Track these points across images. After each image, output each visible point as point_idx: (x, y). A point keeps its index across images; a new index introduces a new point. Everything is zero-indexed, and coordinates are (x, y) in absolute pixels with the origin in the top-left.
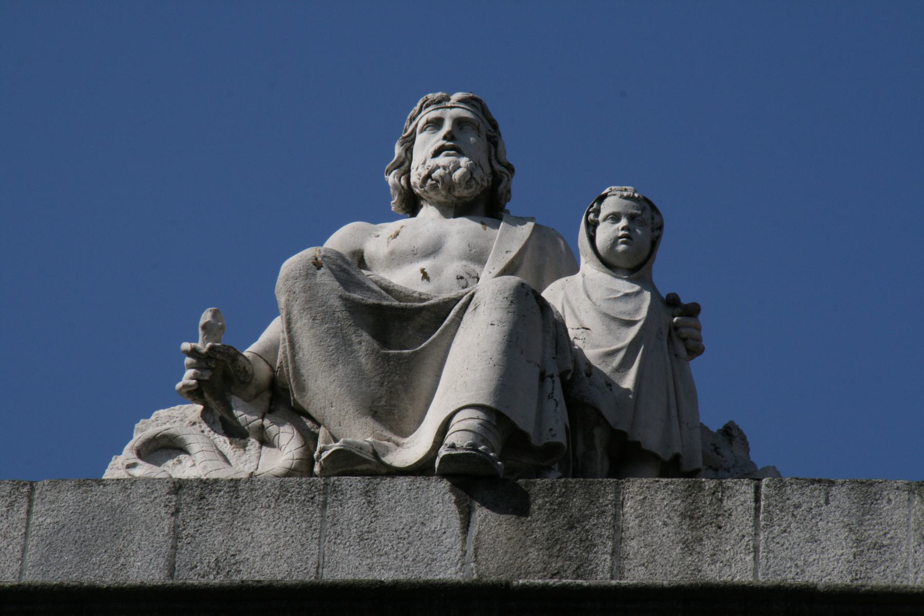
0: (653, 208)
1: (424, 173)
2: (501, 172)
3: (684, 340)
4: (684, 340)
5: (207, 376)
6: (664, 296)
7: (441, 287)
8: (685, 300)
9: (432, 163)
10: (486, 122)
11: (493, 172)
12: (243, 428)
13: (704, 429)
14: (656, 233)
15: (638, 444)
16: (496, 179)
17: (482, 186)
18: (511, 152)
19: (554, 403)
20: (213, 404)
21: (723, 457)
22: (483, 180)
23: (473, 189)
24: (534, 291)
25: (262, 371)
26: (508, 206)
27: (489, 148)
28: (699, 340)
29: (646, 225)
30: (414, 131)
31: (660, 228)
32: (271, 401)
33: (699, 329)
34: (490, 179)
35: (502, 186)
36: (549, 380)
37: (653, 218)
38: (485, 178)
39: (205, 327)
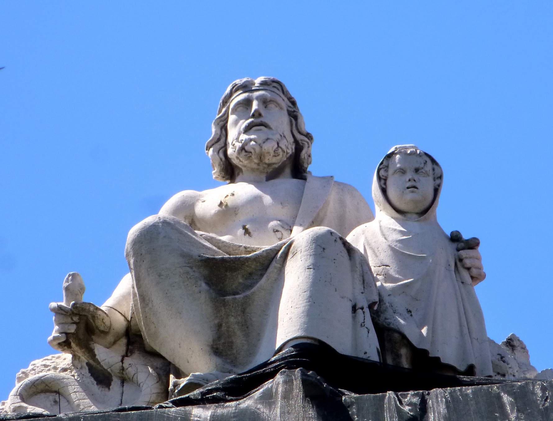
0: (433, 161)
1: (238, 145)
2: (301, 140)
3: (469, 269)
4: (469, 269)
5: (72, 329)
6: (449, 234)
7: (262, 244)
8: (466, 236)
9: (244, 137)
10: (286, 99)
11: (296, 141)
12: (106, 370)
13: (492, 342)
14: (438, 182)
15: (438, 359)
16: (299, 148)
17: (287, 153)
18: (308, 123)
19: (366, 330)
20: (80, 353)
21: (508, 364)
22: (288, 148)
23: (281, 156)
24: (341, 239)
25: (119, 322)
26: (310, 168)
27: (291, 122)
28: (480, 268)
29: (429, 176)
30: (227, 112)
31: (441, 177)
32: (129, 343)
33: (479, 259)
34: (293, 147)
35: (304, 152)
36: (360, 311)
37: (434, 170)
38: (290, 147)
39: (67, 289)
